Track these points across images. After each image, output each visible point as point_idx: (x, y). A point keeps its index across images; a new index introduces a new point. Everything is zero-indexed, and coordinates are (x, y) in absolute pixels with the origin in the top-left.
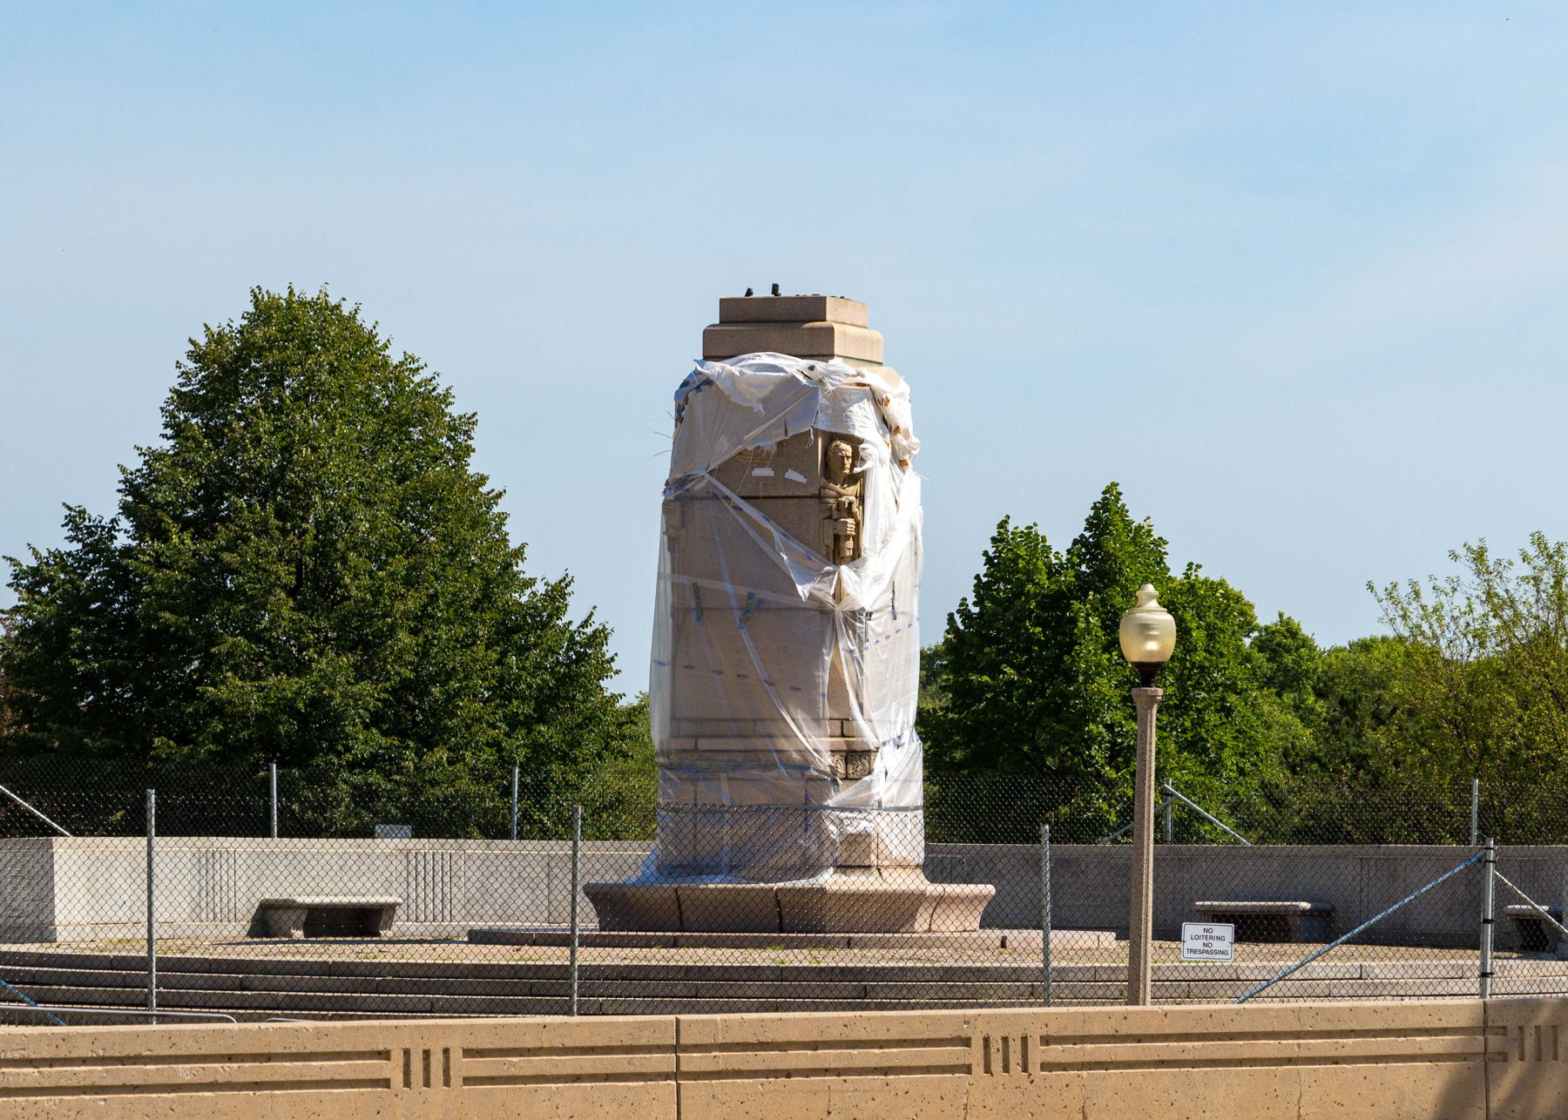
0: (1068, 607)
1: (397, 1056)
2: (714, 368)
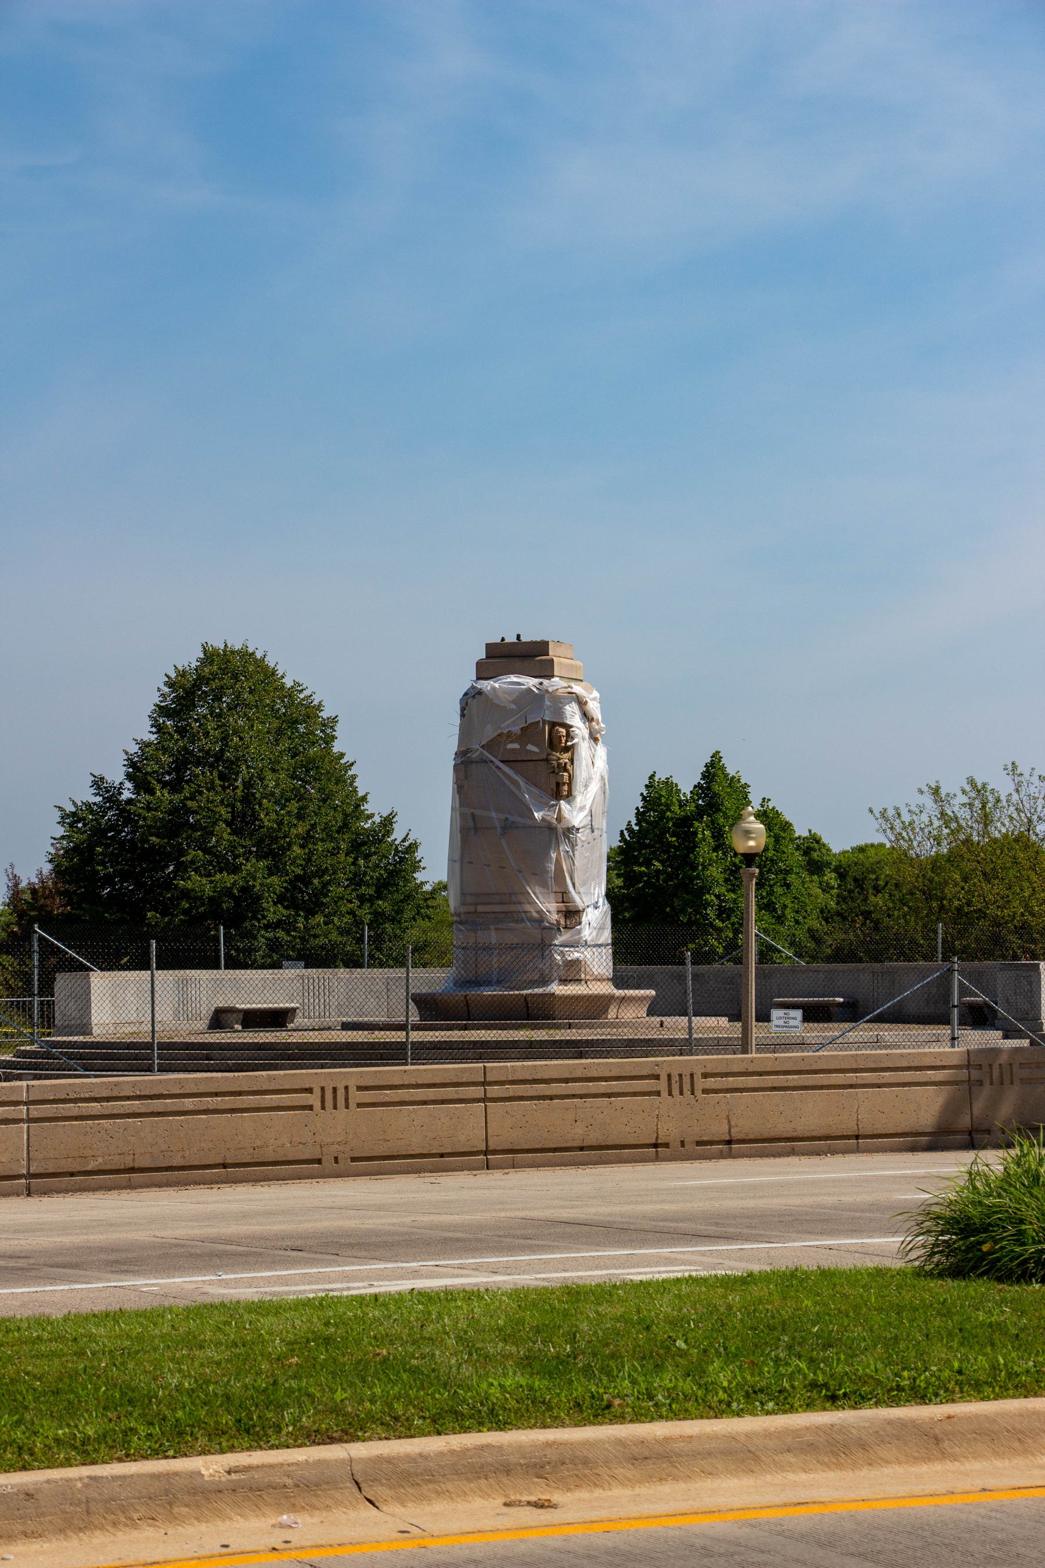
0: (692, 825)
1: (317, 1092)
2: (486, 685)
